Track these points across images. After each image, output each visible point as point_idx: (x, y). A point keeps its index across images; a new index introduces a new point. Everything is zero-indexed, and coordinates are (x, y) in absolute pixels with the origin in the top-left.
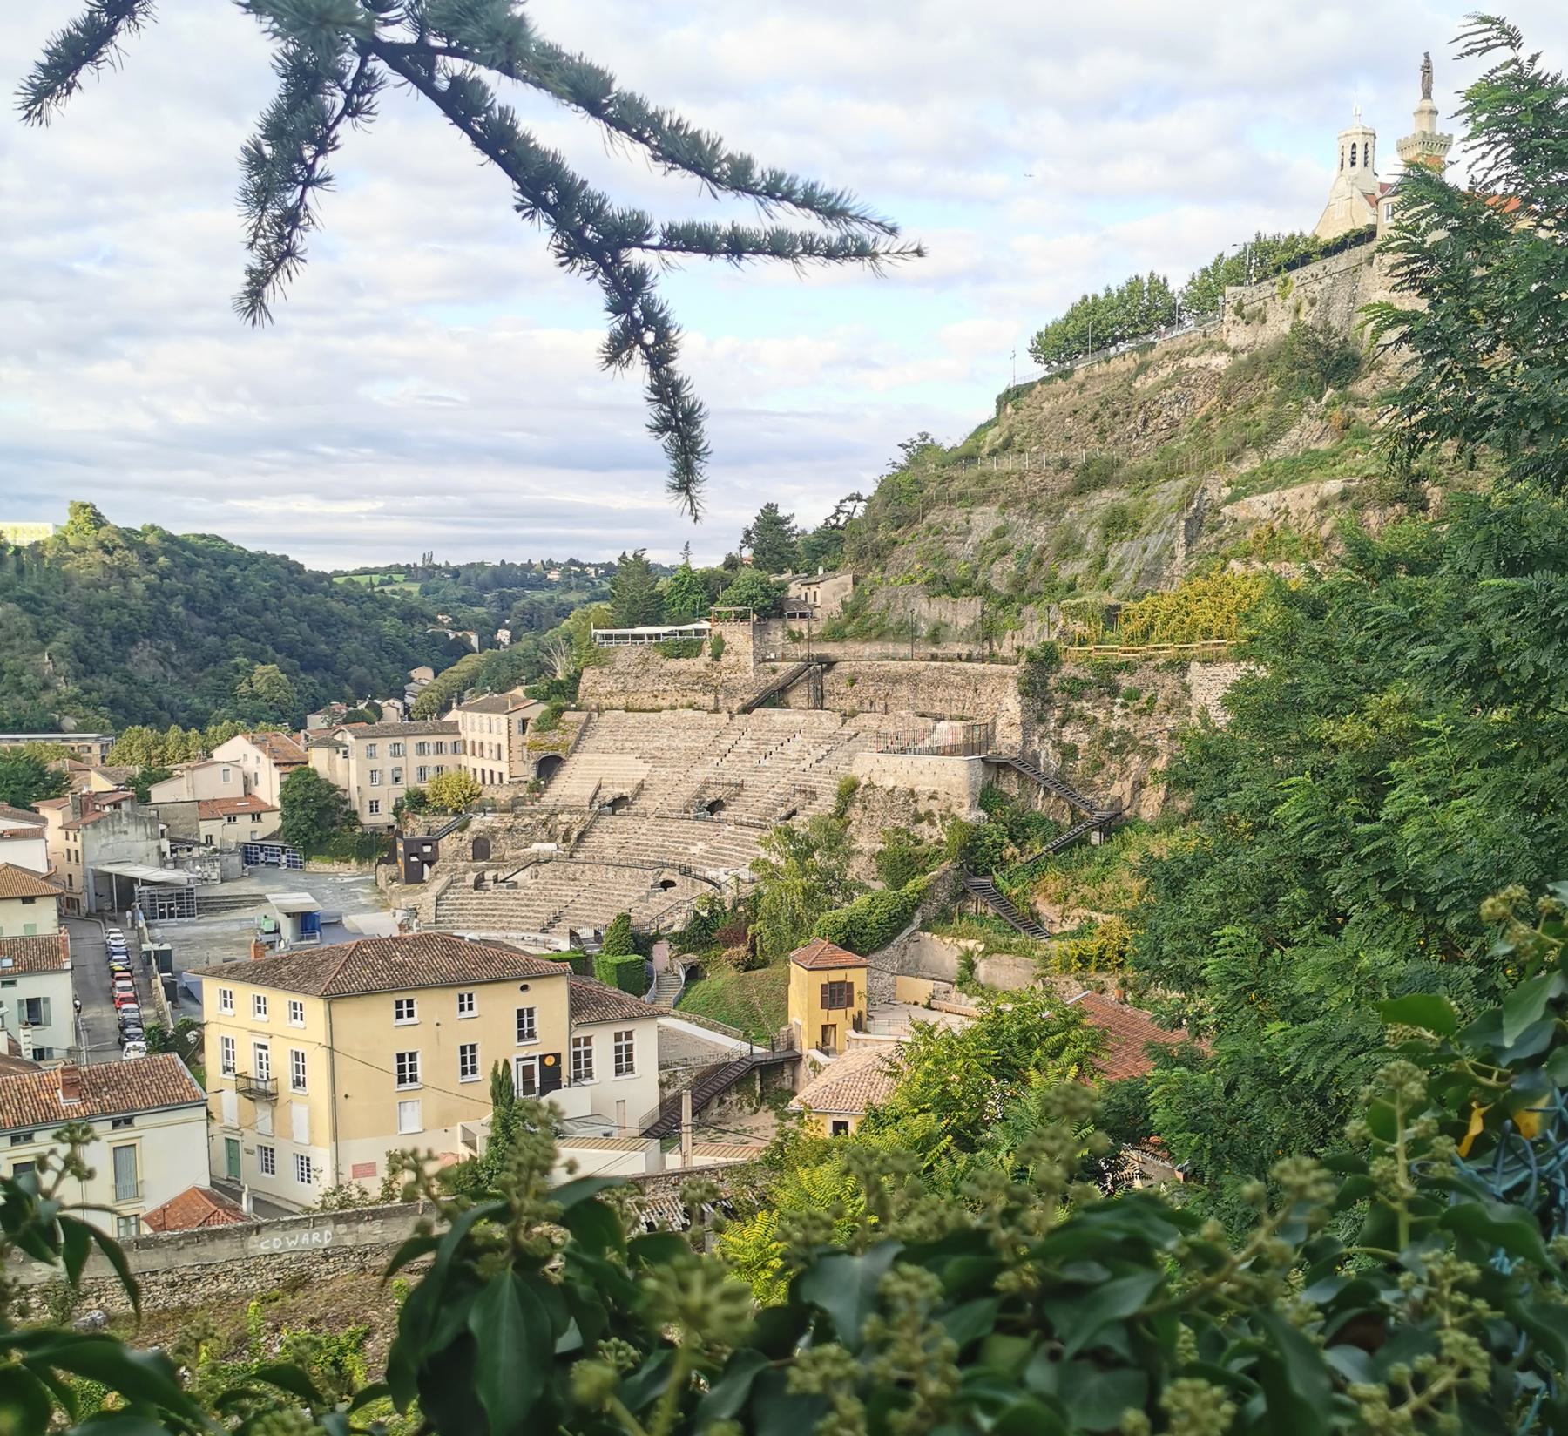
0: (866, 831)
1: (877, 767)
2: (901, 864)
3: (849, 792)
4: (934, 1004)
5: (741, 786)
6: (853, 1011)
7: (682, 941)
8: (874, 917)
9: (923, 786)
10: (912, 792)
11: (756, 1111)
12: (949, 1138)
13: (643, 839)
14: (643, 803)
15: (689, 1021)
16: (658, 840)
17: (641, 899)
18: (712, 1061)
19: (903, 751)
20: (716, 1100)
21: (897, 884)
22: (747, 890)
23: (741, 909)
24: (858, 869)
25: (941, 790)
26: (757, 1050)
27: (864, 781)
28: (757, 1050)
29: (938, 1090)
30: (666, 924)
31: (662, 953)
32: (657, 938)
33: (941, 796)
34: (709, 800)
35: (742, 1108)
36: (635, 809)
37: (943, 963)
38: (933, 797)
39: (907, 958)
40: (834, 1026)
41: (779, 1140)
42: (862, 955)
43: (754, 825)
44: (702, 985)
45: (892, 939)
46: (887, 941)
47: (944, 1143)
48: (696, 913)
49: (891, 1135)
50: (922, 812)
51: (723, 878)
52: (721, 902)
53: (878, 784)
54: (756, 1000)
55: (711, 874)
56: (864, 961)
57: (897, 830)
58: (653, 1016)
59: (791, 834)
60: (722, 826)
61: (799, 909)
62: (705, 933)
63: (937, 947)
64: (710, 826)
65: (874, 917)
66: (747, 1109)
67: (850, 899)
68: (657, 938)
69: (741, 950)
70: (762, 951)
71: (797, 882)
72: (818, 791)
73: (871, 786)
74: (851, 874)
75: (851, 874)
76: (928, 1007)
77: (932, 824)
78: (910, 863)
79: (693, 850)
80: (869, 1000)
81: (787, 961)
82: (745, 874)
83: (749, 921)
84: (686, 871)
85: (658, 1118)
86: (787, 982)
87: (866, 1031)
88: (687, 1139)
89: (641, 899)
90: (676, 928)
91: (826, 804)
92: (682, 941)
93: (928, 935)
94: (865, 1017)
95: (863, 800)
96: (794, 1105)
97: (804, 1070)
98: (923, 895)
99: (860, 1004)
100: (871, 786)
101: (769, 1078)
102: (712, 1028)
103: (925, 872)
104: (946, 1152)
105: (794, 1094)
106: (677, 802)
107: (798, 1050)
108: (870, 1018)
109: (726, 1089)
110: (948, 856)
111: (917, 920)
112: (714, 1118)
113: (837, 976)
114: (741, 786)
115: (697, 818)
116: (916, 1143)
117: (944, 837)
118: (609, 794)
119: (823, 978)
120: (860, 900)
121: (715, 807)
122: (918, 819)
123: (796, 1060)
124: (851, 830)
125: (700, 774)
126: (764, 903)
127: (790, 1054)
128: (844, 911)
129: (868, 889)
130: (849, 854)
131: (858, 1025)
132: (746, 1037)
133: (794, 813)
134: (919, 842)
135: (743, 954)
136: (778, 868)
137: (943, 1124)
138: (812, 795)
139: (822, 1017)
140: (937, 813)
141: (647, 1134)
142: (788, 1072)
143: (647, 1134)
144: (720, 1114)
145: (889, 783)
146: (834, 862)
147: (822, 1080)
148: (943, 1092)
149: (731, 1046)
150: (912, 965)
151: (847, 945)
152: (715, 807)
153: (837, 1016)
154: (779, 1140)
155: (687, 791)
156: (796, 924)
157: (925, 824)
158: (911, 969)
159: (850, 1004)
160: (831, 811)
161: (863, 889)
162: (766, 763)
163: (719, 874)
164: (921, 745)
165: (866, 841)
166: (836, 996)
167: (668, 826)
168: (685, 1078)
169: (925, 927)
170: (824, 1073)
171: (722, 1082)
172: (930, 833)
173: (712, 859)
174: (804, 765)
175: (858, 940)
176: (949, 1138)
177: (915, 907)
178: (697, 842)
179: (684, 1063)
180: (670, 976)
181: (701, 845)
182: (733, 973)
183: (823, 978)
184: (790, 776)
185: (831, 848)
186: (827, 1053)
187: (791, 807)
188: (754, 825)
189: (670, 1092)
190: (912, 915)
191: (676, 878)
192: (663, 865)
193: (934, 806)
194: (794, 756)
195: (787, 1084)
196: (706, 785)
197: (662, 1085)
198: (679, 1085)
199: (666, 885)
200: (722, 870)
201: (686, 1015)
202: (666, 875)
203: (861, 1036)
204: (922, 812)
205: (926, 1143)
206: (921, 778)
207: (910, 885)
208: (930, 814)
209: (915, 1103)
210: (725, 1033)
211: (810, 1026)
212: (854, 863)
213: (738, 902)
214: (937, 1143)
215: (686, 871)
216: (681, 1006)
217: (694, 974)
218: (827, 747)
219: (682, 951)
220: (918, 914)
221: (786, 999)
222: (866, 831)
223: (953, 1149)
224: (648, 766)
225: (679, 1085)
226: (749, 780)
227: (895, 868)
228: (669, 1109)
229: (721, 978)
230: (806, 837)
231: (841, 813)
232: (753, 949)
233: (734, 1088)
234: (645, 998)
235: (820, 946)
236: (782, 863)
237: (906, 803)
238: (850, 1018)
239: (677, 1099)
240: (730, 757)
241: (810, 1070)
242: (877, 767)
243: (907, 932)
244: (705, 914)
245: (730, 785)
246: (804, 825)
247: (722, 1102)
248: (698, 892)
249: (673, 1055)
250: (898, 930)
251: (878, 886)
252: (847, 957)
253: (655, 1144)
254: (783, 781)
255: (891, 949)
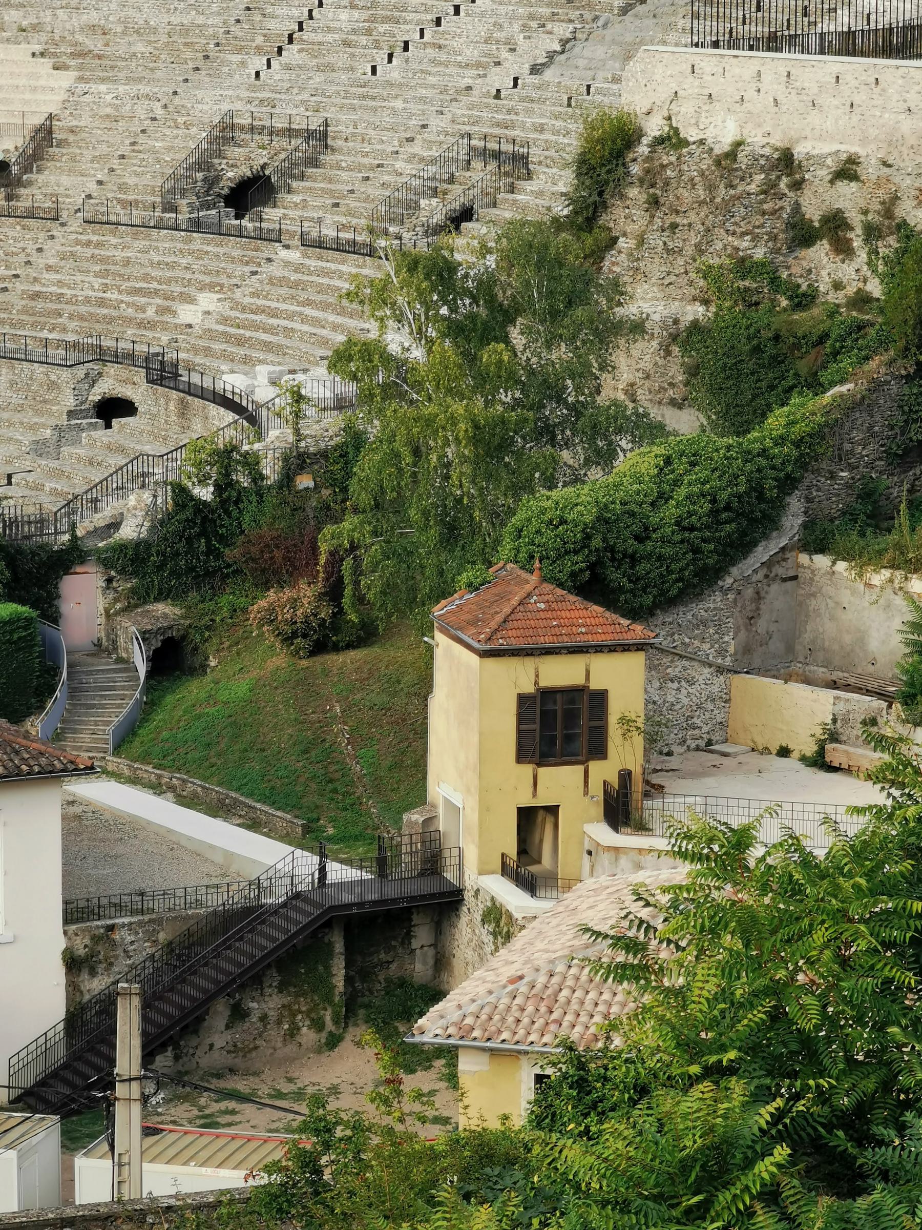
0: (655, 268)
1: (690, 86)
2: (753, 353)
3: (609, 155)
4: (835, 753)
5: (320, 137)
6: (604, 772)
7: (139, 568)
8: (670, 511)
9: (820, 139)
10: (786, 161)
11: (333, 1042)
12: (781, 1152)
13: (49, 283)
14: (51, 182)
15: (157, 788)
16: (90, 285)
17: (40, 449)
18: (215, 901)
19: (773, 42)
20: (221, 1010)
21: (739, 415)
22: (322, 429)
23: (305, 481)
24: (631, 373)
25: (870, 155)
26: (338, 872)
27: (654, 127)
28: (338, 872)
29: (758, 1015)
30: (100, 519)
31: (85, 601)
32: (70, 558)
33: (870, 170)
34: (230, 176)
35: (293, 1032)
36: (27, 197)
37: (861, 640)
38: (847, 171)
39: (762, 625)
40: (553, 810)
41: (308, 1143)
42: (635, 614)
43: (353, 248)
44: (193, 690)
45: (719, 572)
46: (703, 578)
47: (765, 1168)
48: (181, 493)
49: (617, 1137)
50: (813, 212)
51: (264, 393)
52: (251, 463)
53: (691, 134)
54: (341, 734)
55: (233, 381)
56: (638, 631)
57: (744, 266)
58: (51, 774)
59: (441, 274)
60: (267, 249)
61: (462, 482)
62: (207, 544)
63: (845, 597)
64: (232, 247)
65: (670, 511)
66: (308, 1035)
67: (606, 458)
68: (70, 558)
69: (303, 597)
70: (360, 599)
71: (459, 408)
72: (535, 154)
73: (672, 140)
74: (612, 390)
75: (612, 390)
76: (819, 762)
77: (843, 249)
78: (776, 361)
79: (187, 314)
80: (651, 740)
81: (428, 629)
82: (320, 384)
83: (329, 514)
84: (163, 373)
85: (60, 1054)
86: (425, 684)
87: (642, 828)
88: (128, 1118)
89: (40, 449)
90: (129, 532)
91: (549, 190)
92: (139, 568)
93: (822, 561)
94: (638, 787)
95: (650, 178)
96: (431, 1026)
97: (468, 930)
98: (811, 451)
99: (625, 753)
100: (672, 140)
101: (378, 946)
102: (219, 809)
103: (816, 386)
104: (771, 1195)
105: (436, 995)
106: (145, 180)
107: (450, 875)
108: (654, 790)
109: (253, 979)
110: (883, 343)
111: (793, 520)
112: (217, 1059)
113: (561, 672)
114: (320, 137)
115: (196, 226)
116: (685, 1167)
117: (875, 288)
118: (235, 167)
119: (521, 676)
120: (634, 461)
121: (250, 194)
122: (803, 235)
123: (449, 902)
124: (616, 263)
125: (210, 103)
126: (366, 466)
127: (426, 886)
128: (581, 491)
129: (656, 431)
130: (609, 332)
131: (619, 810)
132: (310, 837)
133: (467, 214)
134: (804, 300)
135: (306, 607)
136: (398, 365)
137: (766, 1112)
138: (516, 165)
139: (519, 785)
140: (855, 218)
141: (31, 1099)
142: (422, 936)
143: (31, 1099)
144: (234, 1049)
145: (722, 132)
146: (561, 353)
147: (510, 961)
148: (777, 1016)
149: (261, 859)
150: (777, 645)
151: (592, 586)
152: (250, 194)
153: (561, 784)
154: (308, 1143)
155: (174, 146)
156: (453, 529)
157: (820, 252)
158: (785, 655)
159: (599, 750)
160: (562, 210)
161: (648, 430)
162: (393, 72)
163: (257, 383)
164: (827, 26)
165: (657, 294)
166: (557, 727)
167: (119, 247)
168: (136, 945)
169: (817, 540)
170: (520, 940)
171: (243, 954)
172: (840, 275)
173: (240, 343)
174: (500, 79)
175: (628, 573)
176: (781, 1152)
177: (788, 484)
178: (200, 297)
179: (138, 902)
180: (105, 664)
181: (208, 300)
182: (279, 660)
183: (521, 676)
184: (459, 110)
185: (554, 315)
186: (530, 885)
187: (457, 198)
188: (353, 248)
189: (95, 985)
190: (779, 505)
191: (136, 389)
192: (103, 356)
193: (848, 198)
194: (471, 53)
195: (420, 969)
196: (225, 133)
197: (74, 964)
198: (121, 965)
199: (112, 409)
200: (263, 372)
201: (148, 771)
202: (110, 384)
203: (626, 840)
204: (813, 212)
205: (718, 1164)
206: (814, 118)
207: (776, 420)
208: (835, 224)
209: (691, 1048)
210: (254, 825)
211: (485, 808)
212: (620, 358)
213: (296, 461)
214: (748, 1164)
215: (163, 373)
216: (136, 746)
217: (171, 659)
218: (563, 30)
219: (140, 598)
220: (795, 504)
221: (422, 732)
222: (655, 268)
223: (791, 1186)
224: (66, 79)
225: (121, 965)
226: (342, 123)
227: (733, 372)
228: (87, 1026)
229: (247, 670)
230: (486, 288)
231: (589, 212)
232: (334, 592)
233: (273, 979)
234: (36, 726)
235: (524, 590)
236: (417, 354)
237: (769, 189)
238: (597, 789)
239: (107, 1006)
240: (292, 53)
241: (484, 934)
242: (690, 86)
243: (763, 553)
244: (205, 493)
245: (290, 133)
246: (484, 250)
247: (238, 1014)
248: (198, 429)
249: (113, 881)
250: (741, 546)
251: (686, 423)
252: (590, 619)
253: (46, 1131)
254: (437, 123)
255: (714, 601)
